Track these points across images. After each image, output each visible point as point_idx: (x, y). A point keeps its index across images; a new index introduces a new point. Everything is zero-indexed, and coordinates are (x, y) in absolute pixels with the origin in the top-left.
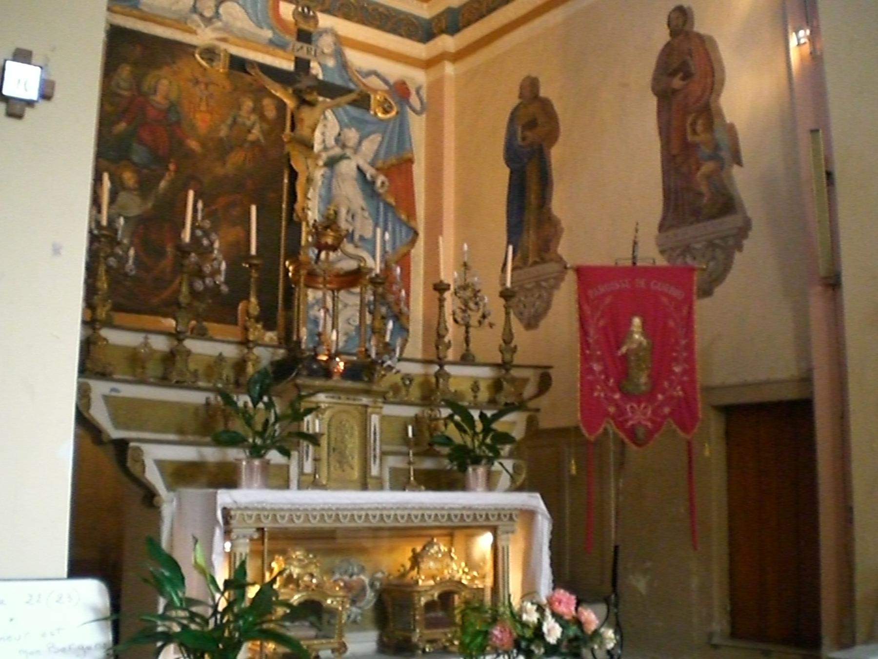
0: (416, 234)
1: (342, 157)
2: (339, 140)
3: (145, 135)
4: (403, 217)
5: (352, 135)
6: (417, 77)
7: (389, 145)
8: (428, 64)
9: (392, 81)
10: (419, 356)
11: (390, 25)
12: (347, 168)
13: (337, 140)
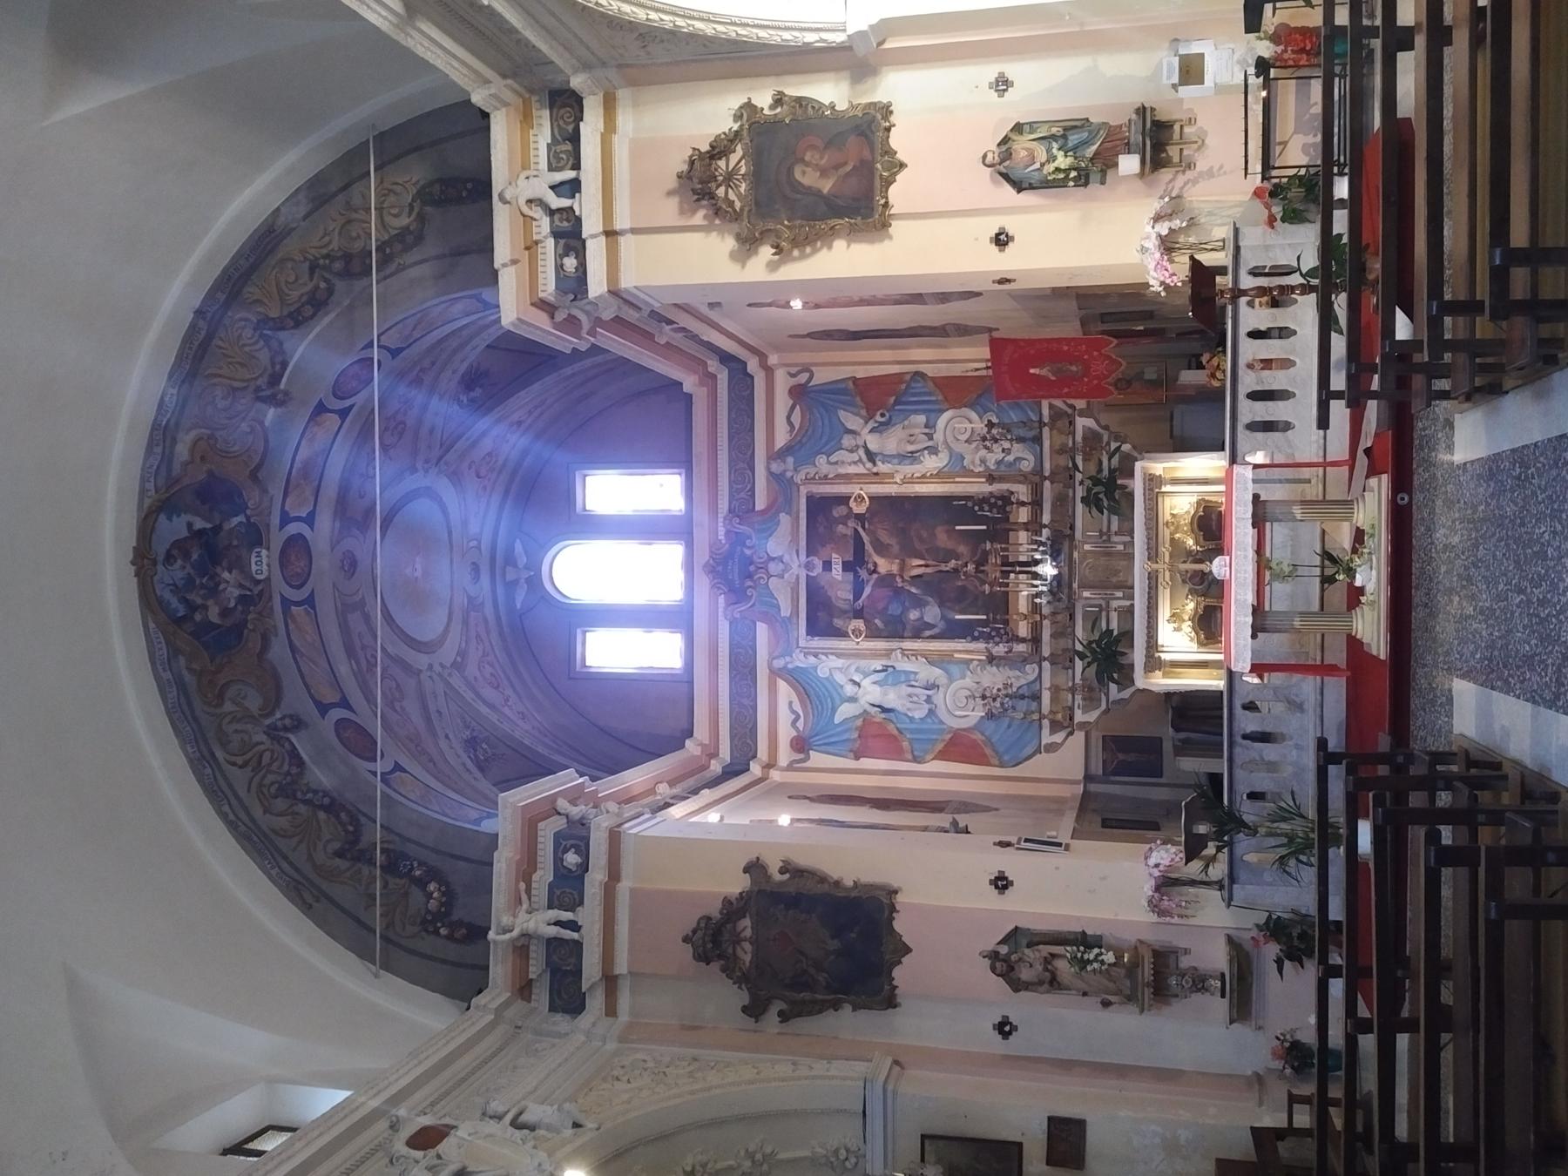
0: (917, 373)
1: (865, 447)
3: (881, 606)
4: (903, 387)
7: (844, 403)
8: (769, 371)
10: (1313, 81)
11: (746, 701)
12: (873, 443)
13: (851, 451)
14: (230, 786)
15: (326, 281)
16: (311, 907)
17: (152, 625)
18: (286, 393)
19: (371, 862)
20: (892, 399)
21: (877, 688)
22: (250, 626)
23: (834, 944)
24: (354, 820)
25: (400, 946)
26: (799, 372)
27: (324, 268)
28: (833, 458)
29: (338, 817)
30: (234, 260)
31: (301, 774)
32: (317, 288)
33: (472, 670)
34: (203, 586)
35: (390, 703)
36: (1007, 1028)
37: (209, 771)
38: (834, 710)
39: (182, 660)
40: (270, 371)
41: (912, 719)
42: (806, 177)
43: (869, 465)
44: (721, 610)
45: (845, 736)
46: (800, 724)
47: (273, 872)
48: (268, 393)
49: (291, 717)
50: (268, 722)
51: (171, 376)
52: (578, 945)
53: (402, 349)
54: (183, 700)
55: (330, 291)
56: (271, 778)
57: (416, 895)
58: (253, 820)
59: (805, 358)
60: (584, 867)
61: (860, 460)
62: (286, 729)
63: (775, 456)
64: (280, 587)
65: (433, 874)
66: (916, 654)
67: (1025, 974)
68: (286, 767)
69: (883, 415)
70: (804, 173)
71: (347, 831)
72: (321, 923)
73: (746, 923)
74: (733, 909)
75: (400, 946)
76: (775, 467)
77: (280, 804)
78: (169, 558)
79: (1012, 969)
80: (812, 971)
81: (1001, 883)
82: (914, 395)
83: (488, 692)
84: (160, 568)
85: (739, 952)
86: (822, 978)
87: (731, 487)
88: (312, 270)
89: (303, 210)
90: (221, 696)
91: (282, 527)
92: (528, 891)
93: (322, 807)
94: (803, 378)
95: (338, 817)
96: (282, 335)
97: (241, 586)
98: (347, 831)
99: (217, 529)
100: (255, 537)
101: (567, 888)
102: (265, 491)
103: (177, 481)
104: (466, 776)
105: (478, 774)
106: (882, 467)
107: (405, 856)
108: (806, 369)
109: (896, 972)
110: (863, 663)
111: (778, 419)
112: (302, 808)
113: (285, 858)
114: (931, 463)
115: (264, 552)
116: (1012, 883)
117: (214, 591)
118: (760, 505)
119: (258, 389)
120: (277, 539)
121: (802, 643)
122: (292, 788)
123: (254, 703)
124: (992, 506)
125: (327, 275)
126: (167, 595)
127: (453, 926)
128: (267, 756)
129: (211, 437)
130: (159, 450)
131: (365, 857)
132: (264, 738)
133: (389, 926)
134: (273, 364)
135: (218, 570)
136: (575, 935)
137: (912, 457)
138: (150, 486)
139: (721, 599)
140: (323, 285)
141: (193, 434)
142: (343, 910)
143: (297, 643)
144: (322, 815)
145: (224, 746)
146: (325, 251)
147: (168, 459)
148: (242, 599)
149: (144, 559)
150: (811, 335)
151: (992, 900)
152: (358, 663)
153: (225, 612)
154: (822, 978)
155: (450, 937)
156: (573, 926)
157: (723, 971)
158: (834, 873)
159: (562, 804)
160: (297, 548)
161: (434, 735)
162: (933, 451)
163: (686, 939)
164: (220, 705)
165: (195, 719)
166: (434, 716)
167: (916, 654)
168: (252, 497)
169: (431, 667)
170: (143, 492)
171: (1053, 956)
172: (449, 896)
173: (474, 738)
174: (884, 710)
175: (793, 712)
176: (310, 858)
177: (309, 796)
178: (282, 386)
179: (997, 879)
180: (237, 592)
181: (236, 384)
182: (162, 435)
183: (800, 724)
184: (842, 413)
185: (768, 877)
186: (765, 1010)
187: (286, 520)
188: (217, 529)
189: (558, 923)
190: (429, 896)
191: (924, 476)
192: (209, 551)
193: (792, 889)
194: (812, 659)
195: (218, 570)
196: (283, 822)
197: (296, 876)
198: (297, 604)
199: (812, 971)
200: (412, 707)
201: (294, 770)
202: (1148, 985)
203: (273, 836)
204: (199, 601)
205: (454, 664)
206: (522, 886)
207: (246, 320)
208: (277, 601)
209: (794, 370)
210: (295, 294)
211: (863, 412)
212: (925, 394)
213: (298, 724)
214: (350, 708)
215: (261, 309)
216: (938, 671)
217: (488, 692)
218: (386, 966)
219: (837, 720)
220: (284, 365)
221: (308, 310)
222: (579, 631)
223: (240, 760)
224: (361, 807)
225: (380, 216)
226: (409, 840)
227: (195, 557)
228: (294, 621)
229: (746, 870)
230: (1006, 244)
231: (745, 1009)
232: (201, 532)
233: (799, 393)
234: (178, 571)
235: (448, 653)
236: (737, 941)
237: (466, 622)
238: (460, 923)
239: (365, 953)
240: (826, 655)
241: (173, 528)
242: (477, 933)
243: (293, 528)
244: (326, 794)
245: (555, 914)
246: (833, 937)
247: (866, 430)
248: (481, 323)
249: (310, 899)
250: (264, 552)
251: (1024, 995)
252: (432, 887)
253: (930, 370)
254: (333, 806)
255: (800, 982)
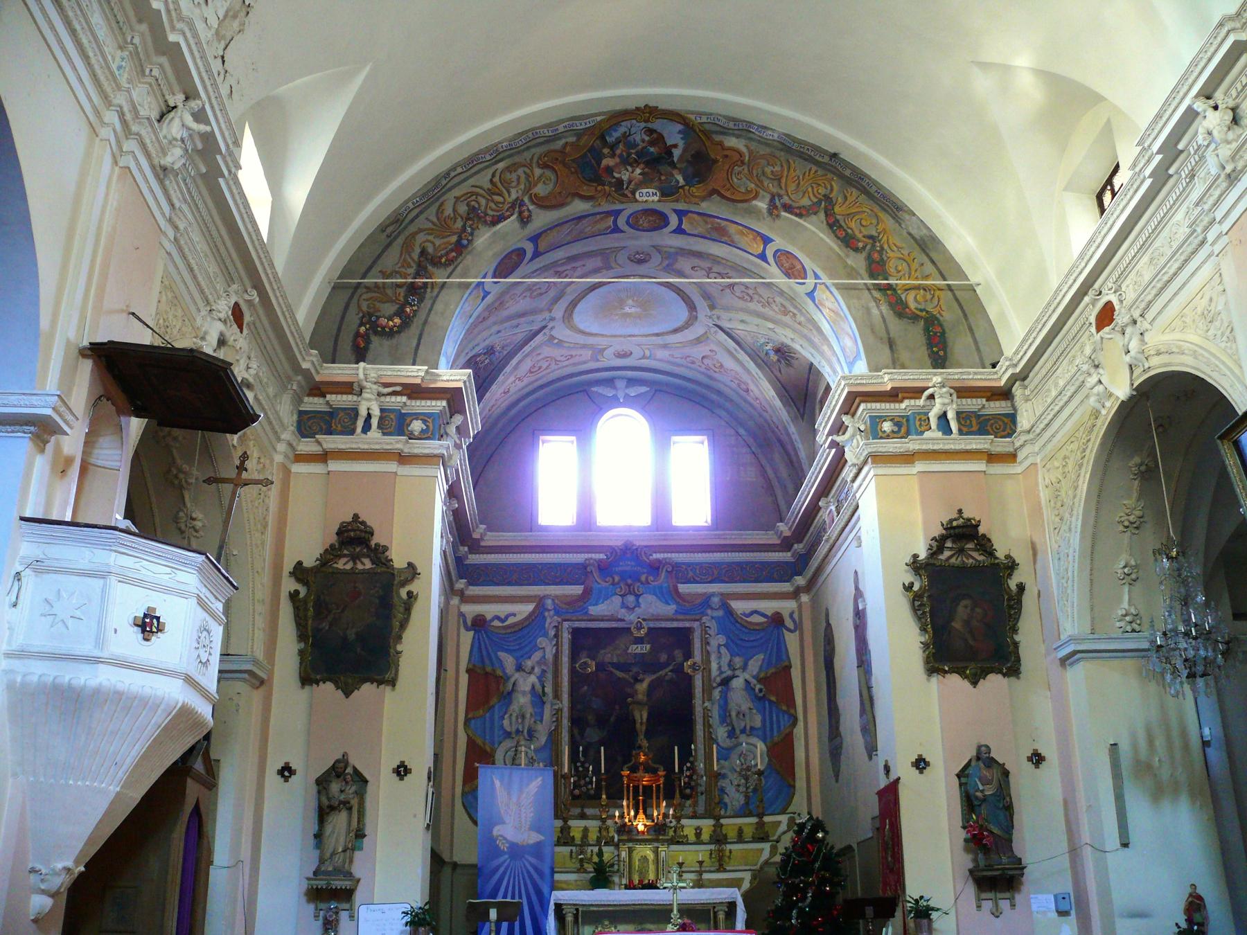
1: (734, 677)
2: (731, 665)
4: (784, 708)
5: (738, 661)
6: (791, 605)
8: (795, 594)
9: (769, 614)
12: (737, 683)
14: (476, 173)
15: (864, 248)
16: (383, 231)
17: (599, 118)
18: (778, 216)
19: (417, 275)
20: (773, 699)
21: (528, 688)
22: (599, 188)
23: (351, 635)
24: (450, 262)
25: (351, 298)
26: (794, 621)
27: (873, 246)
28: (723, 650)
29: (452, 250)
30: (875, 183)
31: (485, 223)
32: (859, 241)
33: (547, 351)
34: (629, 155)
35: (530, 288)
36: (286, 774)
37: (488, 158)
38: (507, 651)
39: (572, 139)
40: (794, 205)
41: (502, 718)
42: (962, 610)
43: (718, 679)
44: (593, 556)
45: (487, 662)
46: (496, 623)
47: (410, 204)
48: (778, 203)
49: (530, 216)
50: (526, 200)
51: (787, 135)
52: (352, 432)
53: (813, 300)
54: (542, 140)
55: (856, 250)
56: (483, 202)
57: (390, 309)
58: (450, 190)
59: (807, 625)
60: (411, 437)
61: (721, 673)
62: (520, 213)
63: (725, 598)
64: (630, 208)
65: (406, 323)
66: (558, 722)
67: (335, 787)
68: (491, 213)
69: (761, 690)
70: (966, 607)
71: (441, 257)
72: (371, 239)
73: (367, 564)
74: (379, 555)
75: (351, 298)
76: (716, 600)
77: (462, 209)
78: (650, 131)
79: (338, 777)
80: (330, 618)
81: (402, 771)
82: (778, 716)
83: (528, 364)
84: (643, 125)
85: (344, 560)
86: (325, 625)
87: (697, 564)
88: (871, 237)
89: (914, 232)
90: (545, 166)
91: (675, 211)
92: (395, 393)
93: (460, 238)
94: (789, 623)
95: (452, 250)
96: (822, 215)
97: (630, 182)
98: (441, 257)
99: (673, 165)
100: (668, 192)
101: (395, 423)
102: (703, 199)
103: (709, 138)
104: (471, 346)
105: (470, 355)
106: (716, 694)
107: (421, 300)
108: (798, 626)
109: (329, 686)
110: (550, 676)
111: (756, 602)
112: (459, 224)
113: (421, 212)
114: (721, 733)
115: (656, 198)
116: (402, 779)
117: (626, 162)
118: (683, 588)
119: (780, 196)
120: (667, 208)
121: (566, 624)
122: (475, 218)
123: (541, 190)
124: (690, 777)
125: (868, 247)
126: (622, 130)
127: (366, 338)
128: (499, 199)
129: (743, 163)
130: (731, 125)
131: (421, 271)
132: (514, 196)
133: (368, 289)
134: (799, 208)
135: (642, 166)
136: (359, 430)
137: (725, 717)
138: (704, 119)
139: (602, 556)
140: (860, 245)
141: (744, 150)
142: (383, 252)
143: (585, 221)
144: (454, 239)
145: (509, 169)
146: (886, 247)
147: (725, 132)
148: (620, 182)
149: (648, 112)
150: (829, 625)
151: (388, 763)
152: (563, 264)
153: (609, 170)
154: (325, 625)
155: (358, 334)
156: (367, 427)
157: (332, 546)
158: (408, 635)
159: (458, 419)
160: (657, 220)
161: (502, 322)
162: (732, 734)
163: (356, 516)
164: (539, 166)
165: (528, 148)
166: (514, 322)
167: (558, 722)
168: (697, 191)
169: (552, 319)
170: (700, 114)
171: (350, 809)
172: (391, 334)
173: (494, 353)
174: (510, 694)
175: (507, 617)
176: (421, 230)
177: (469, 230)
178: (783, 214)
179: (406, 767)
180: (625, 177)
181: (783, 181)
182: (744, 128)
183: (496, 623)
184: (761, 656)
185: (404, 584)
186: (298, 580)
187: (681, 214)
188: (673, 165)
189: (369, 416)
190: (390, 319)
191: (710, 726)
192: (656, 160)
193: (396, 600)
194: (552, 633)
195: (642, 166)
196: (448, 211)
197: (407, 221)
198: (615, 222)
199: (330, 618)
200: (523, 304)
201: (488, 219)
202: (328, 884)
203: (437, 204)
204: (618, 152)
205: (553, 338)
206: (398, 389)
207: (832, 190)
208: (618, 207)
209: (796, 616)
210: (853, 225)
211: (762, 675)
212: (779, 727)
213: (524, 221)
214: (532, 259)
215: (840, 200)
216: (543, 739)
217: (528, 364)
218: (336, 288)
219: (501, 654)
220: (800, 215)
221: (842, 234)
222: (574, 438)
223: (496, 179)
224: (459, 268)
225: (918, 288)
226: (434, 302)
227: (652, 149)
228: (602, 219)
229: (410, 564)
230: (918, 768)
231: (300, 563)
232: (670, 154)
233: (777, 620)
234: (639, 137)
235: (561, 332)
236: (355, 558)
237: (584, 346)
238: (368, 342)
239: (346, 272)
240: (557, 644)
241: (673, 134)
242: (360, 354)
243: (674, 221)
244: (470, 242)
245: (376, 412)
246: (357, 634)
247: (747, 677)
248: (834, 360)
249: (389, 230)
250: (656, 198)
251: (314, 789)
252: (397, 320)
253: (799, 731)
254: (460, 248)
255: (321, 607)
